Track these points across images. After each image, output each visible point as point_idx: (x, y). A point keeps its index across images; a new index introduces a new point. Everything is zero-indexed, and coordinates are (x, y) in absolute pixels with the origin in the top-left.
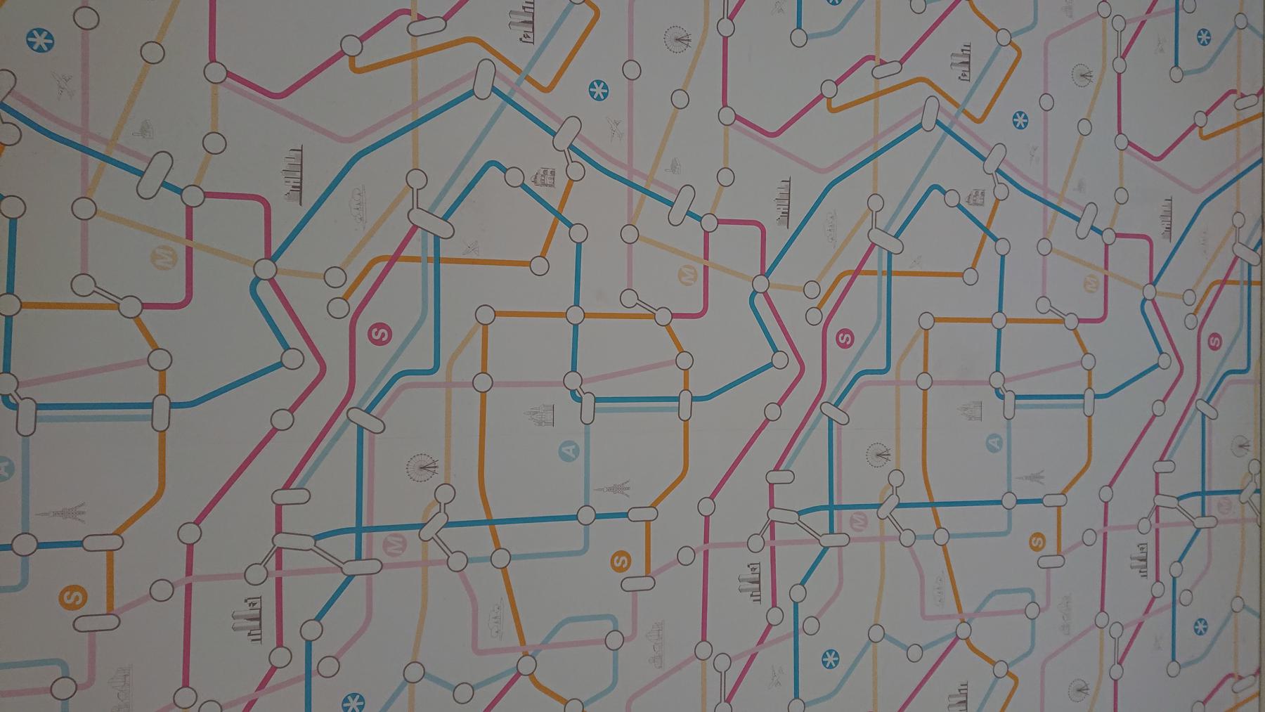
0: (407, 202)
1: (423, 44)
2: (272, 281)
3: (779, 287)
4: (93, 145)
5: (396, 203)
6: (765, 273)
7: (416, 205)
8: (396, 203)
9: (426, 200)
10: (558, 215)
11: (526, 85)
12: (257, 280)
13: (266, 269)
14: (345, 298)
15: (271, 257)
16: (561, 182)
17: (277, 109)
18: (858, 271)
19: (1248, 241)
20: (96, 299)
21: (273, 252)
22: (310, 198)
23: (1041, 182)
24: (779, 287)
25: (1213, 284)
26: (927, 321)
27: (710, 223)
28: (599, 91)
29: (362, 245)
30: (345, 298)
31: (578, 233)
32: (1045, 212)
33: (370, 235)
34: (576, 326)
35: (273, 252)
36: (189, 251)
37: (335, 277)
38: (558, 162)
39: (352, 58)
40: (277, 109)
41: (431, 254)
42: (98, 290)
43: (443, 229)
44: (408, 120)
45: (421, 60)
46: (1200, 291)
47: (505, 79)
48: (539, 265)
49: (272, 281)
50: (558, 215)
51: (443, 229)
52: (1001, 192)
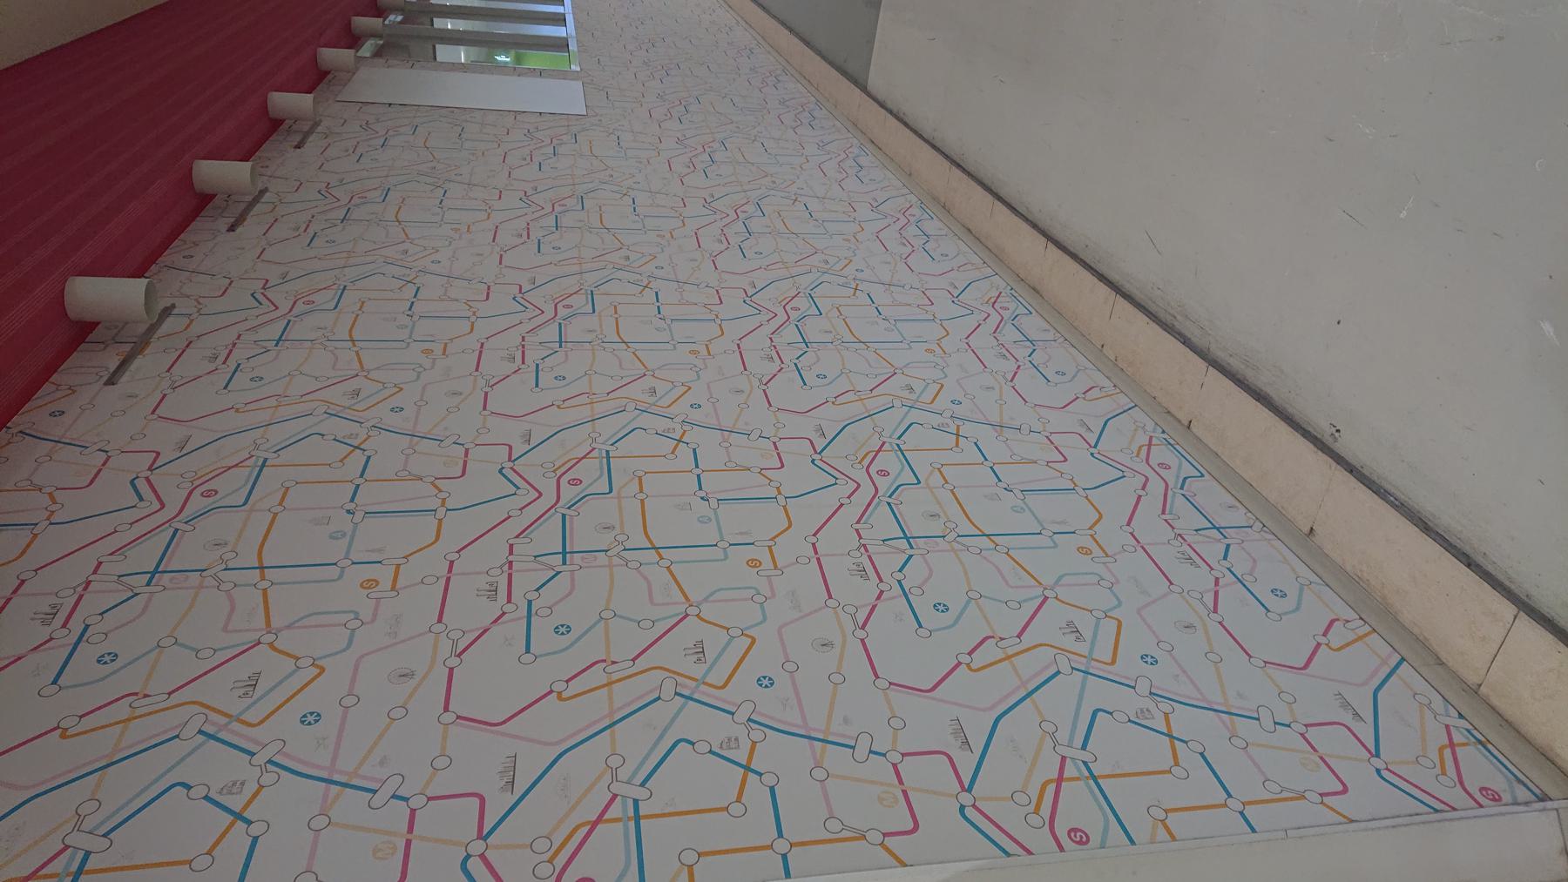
0: (607, 778)
1: (615, 677)
2: (482, 856)
3: (497, 847)
4: (813, 735)
5: (599, 778)
6: (481, 836)
7: (1056, 743)
8: (599, 778)
9: (623, 774)
10: (747, 768)
11: (703, 688)
12: (468, 856)
13: (966, 799)
14: (550, 861)
15: (481, 836)
16: (746, 745)
17: (503, 734)
18: (1060, 780)
19: (1071, 739)
20: (846, 834)
21: (485, 832)
22: (520, 788)
23: (799, 722)
24: (497, 847)
25: (1441, 750)
26: (689, 858)
27: (896, 758)
28: (766, 682)
29: (567, 815)
30: (550, 861)
31: (769, 780)
32: (812, 747)
33: (573, 808)
34: (784, 856)
35: (485, 832)
36: (408, 843)
37: (542, 845)
38: (741, 732)
39: (560, 693)
40: (503, 734)
41: (631, 813)
42: (845, 827)
43: (641, 793)
44: (607, 722)
45: (234, 712)
46: (1034, 793)
47: (685, 686)
48: (736, 809)
49: (482, 856)
50: (747, 768)
51: (641, 793)
52: (757, 735)
